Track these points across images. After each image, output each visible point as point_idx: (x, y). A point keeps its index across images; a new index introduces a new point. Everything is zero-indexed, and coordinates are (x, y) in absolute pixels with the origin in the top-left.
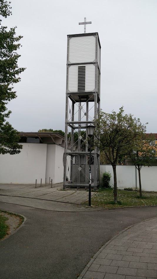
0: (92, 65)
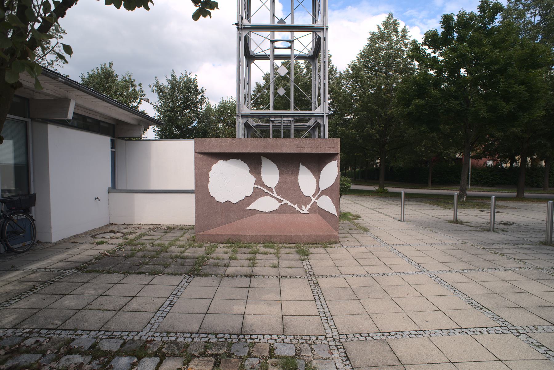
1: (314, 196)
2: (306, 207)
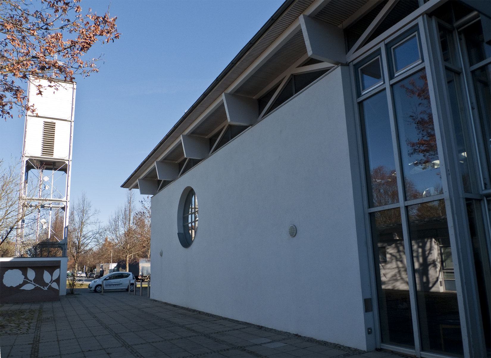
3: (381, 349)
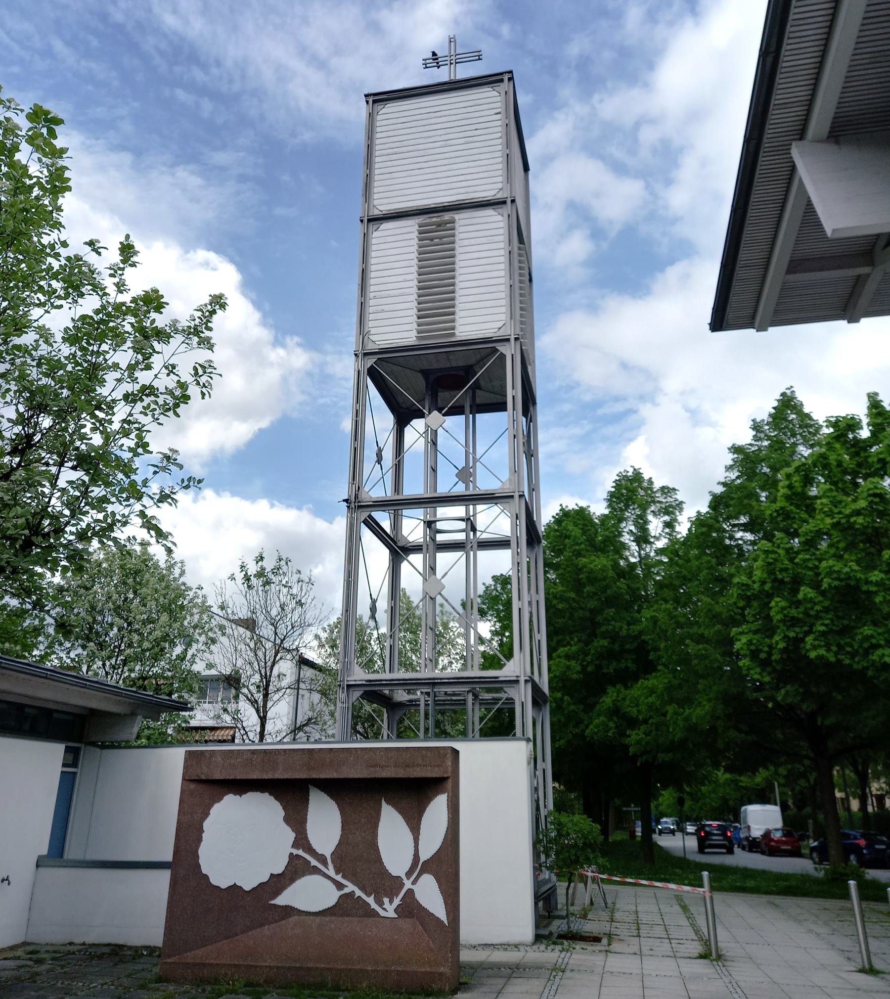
0: (489, 212)
1: (409, 874)
2: (391, 902)
3: (686, 411)
